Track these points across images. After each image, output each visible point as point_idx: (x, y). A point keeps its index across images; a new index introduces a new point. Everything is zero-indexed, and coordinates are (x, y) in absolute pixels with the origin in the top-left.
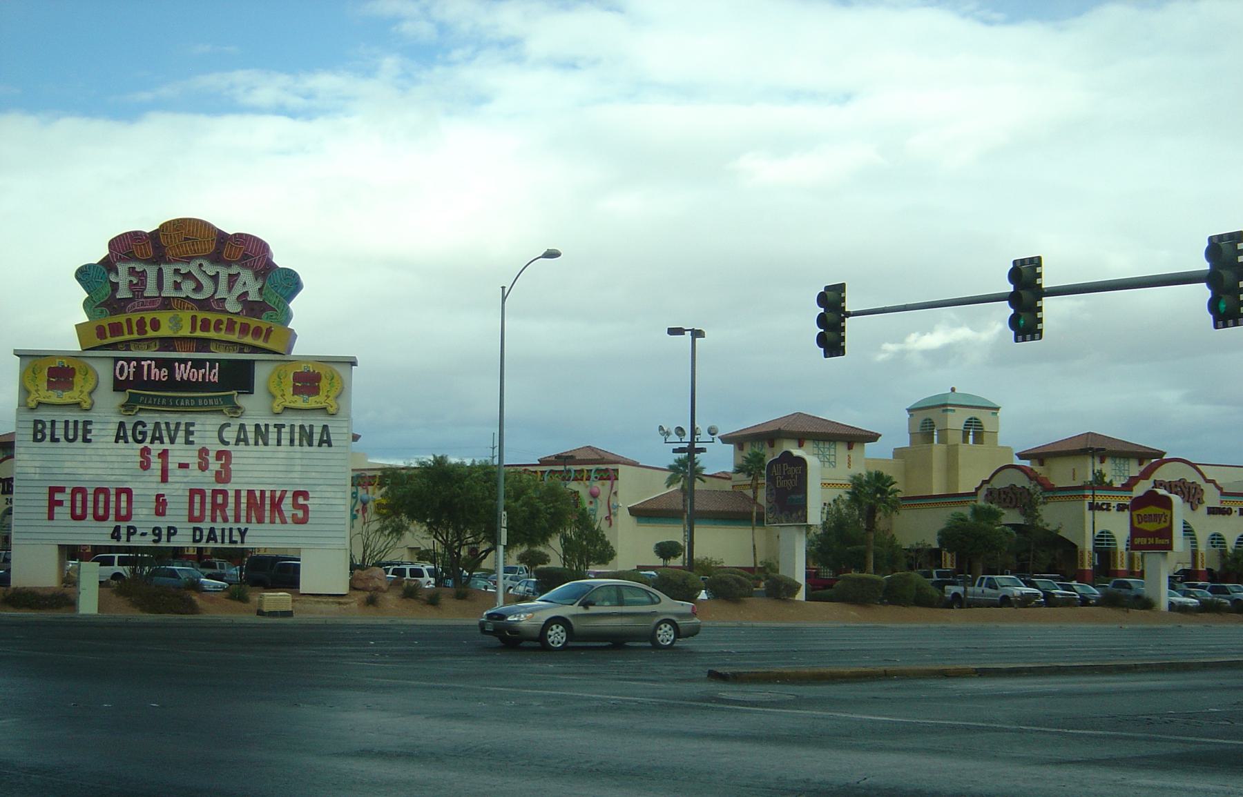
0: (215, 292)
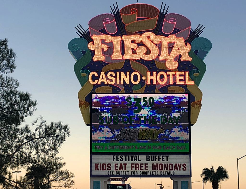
0: (159, 55)
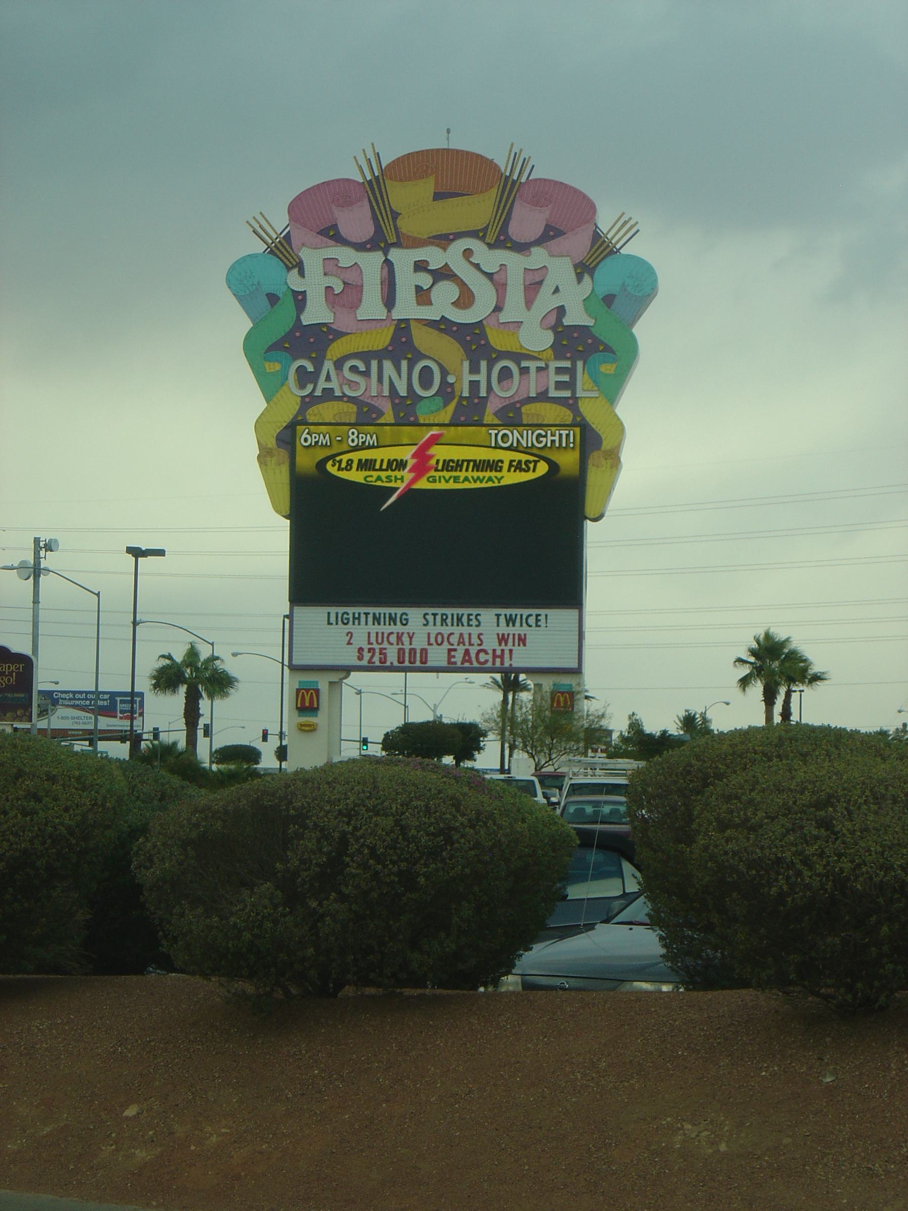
0: (498, 309)
